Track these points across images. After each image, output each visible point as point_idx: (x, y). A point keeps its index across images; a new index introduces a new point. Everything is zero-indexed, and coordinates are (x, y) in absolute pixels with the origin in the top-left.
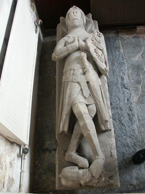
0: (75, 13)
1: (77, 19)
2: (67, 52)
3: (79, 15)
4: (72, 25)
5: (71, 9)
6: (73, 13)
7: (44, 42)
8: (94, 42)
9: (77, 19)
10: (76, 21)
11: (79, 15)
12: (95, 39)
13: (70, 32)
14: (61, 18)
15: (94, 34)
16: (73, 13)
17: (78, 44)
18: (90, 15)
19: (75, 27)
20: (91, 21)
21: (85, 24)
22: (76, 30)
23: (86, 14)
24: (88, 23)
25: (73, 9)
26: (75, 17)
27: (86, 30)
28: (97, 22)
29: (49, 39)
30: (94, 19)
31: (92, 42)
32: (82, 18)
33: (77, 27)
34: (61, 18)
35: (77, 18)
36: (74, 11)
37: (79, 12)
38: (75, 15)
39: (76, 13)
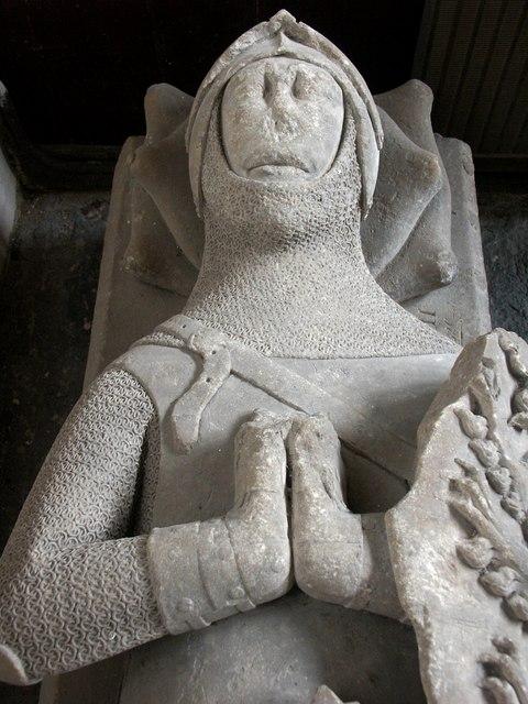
0: (284, 91)
1: (299, 165)
2: (145, 634)
3: (327, 119)
4: (243, 218)
5: (251, 41)
6: (269, 90)
7: (26, 234)
8: (482, 552)
9: (299, 165)
10: (291, 179)
11: (327, 119)
12: (495, 486)
13: (221, 276)
14: (160, 95)
15: (477, 410)
16: (269, 90)
17: (284, 560)
18: (422, 96)
19: (277, 240)
20: (431, 171)
21: (370, 202)
22: (280, 270)
23: (383, 75)
24: (399, 173)
25: (267, 46)
26: (275, 141)
27: (371, 251)
28: (465, 151)
29: (60, 218)
30: (445, 124)
31: (454, 536)
32: (349, 148)
33: (296, 239)
34: (160, 95)
35: (298, 148)
36: (278, 65)
37: (326, 85)
38: (279, 117)
39: (296, 92)
